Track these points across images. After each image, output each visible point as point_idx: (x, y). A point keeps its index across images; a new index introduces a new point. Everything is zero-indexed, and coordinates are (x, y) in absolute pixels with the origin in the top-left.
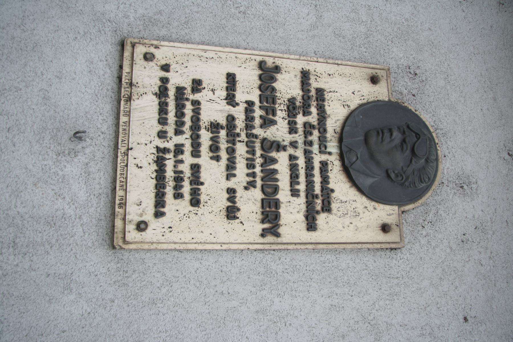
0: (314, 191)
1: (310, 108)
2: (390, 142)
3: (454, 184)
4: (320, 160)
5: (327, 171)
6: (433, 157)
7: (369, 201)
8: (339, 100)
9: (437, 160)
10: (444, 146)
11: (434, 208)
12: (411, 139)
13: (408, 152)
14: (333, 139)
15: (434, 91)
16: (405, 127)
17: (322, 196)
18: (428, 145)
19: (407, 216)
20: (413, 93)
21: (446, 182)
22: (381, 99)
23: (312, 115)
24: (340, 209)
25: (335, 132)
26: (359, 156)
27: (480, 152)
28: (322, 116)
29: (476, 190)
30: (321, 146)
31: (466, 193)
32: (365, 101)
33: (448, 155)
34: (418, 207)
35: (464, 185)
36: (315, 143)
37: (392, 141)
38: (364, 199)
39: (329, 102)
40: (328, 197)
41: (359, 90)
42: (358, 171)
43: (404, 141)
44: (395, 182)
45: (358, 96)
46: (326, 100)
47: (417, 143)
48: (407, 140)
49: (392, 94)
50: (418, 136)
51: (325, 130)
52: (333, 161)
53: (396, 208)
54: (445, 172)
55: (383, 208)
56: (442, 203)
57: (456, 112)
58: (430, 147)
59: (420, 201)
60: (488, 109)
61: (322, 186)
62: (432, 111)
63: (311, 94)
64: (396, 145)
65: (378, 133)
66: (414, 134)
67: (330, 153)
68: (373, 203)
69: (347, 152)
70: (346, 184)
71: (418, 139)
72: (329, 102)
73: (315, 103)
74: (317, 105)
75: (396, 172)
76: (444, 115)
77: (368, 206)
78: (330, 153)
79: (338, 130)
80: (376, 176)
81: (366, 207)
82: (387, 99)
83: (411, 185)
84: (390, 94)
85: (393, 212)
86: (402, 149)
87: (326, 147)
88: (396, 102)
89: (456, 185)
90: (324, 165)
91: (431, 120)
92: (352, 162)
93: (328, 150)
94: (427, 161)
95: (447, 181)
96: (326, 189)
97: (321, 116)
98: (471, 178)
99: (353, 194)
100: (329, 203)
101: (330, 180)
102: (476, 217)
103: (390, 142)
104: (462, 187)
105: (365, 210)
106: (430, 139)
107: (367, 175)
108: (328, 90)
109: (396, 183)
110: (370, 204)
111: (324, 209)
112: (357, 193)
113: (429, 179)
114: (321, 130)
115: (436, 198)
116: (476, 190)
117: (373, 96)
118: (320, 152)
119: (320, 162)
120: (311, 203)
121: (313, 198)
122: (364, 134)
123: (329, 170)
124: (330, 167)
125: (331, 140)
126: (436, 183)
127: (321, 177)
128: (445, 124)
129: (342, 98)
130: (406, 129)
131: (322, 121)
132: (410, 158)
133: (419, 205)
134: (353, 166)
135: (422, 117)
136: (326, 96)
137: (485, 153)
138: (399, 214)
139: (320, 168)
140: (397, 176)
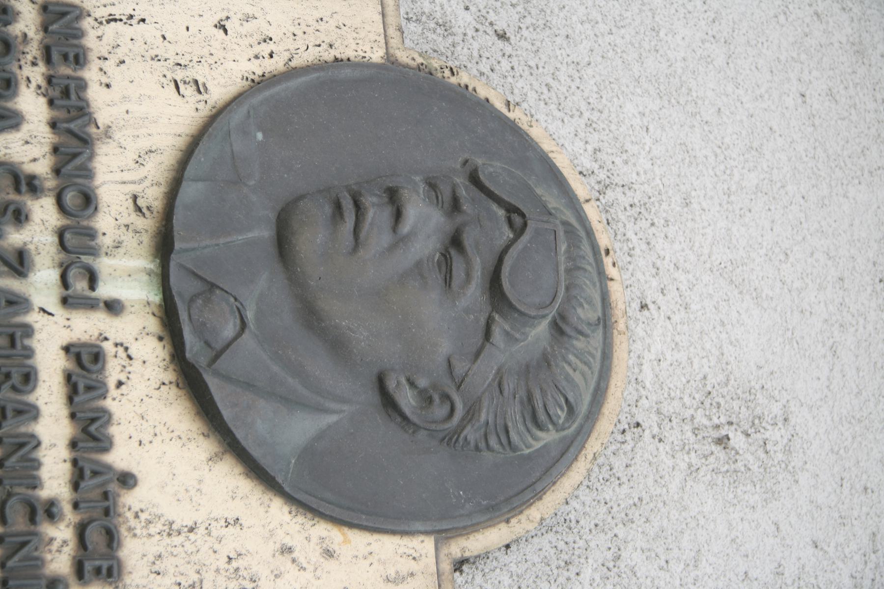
0: (35, 483)
1: (15, 94)
2: (393, 247)
3: (687, 428)
4: (67, 337)
5: (98, 389)
6: (586, 313)
7: (300, 519)
8: (155, 58)
9: (605, 322)
10: (641, 262)
11: (601, 540)
12: (488, 231)
13: (473, 294)
14: (129, 239)
15: (595, 15)
16: (461, 181)
17: (76, 506)
18: (562, 258)
19: (479, 579)
20: (500, 26)
21: (650, 422)
22: (350, 53)
23: (25, 127)
24: (167, 564)
25: (138, 209)
26: (250, 315)
27: (797, 284)
28: (75, 134)
29: (788, 451)
30: (72, 273)
31: (740, 465)
32: (277, 65)
33: (660, 299)
34: (528, 538)
35: (724, 435)
36: (38, 260)
37: (399, 242)
38: (278, 511)
39: (106, 65)
40: (107, 512)
41: (249, 10)
42: (249, 386)
43: (456, 241)
44: (417, 427)
45: (246, 42)
46: (92, 56)
47: (513, 252)
48: (468, 241)
49: (400, 29)
50: (517, 220)
51: (88, 200)
52: (128, 340)
53: (425, 545)
54: (648, 377)
55: (365, 550)
56: (634, 514)
57: (690, 108)
58: (574, 269)
59: (535, 512)
60: (830, 93)
61: (75, 462)
62: (583, 106)
63: (16, 29)
64: (418, 264)
65: (338, 207)
66: (501, 213)
67: (113, 307)
68: (322, 529)
69: (192, 300)
70: (192, 445)
71: (519, 232)
72: (106, 65)
73: (37, 74)
74: (49, 80)
75: (423, 383)
76: (637, 121)
77: (296, 541)
78: (113, 307)
79: (153, 196)
80: (333, 406)
81: (286, 550)
82: (377, 56)
83: (493, 442)
84: (391, 31)
85: (413, 566)
86: (448, 280)
87: (93, 279)
88: (419, 68)
89: (695, 431)
90: (85, 360)
91: (579, 144)
92: (218, 346)
93: (105, 290)
94: (559, 328)
95: (654, 417)
96: (95, 473)
97: (70, 132)
98: (761, 398)
99: (225, 487)
100: (111, 538)
101: (113, 430)
102: (790, 571)
103: (393, 247)
104: (722, 441)
105: (284, 563)
106: (570, 231)
107: (290, 402)
108: (102, 13)
109: (422, 435)
110: (308, 534)
111: (88, 566)
112: (245, 486)
113: (571, 410)
114: (70, 197)
115: (608, 494)
116: (788, 451)
117: (312, 40)
118: (65, 301)
119: (67, 349)
120: (24, 544)
121: (32, 518)
122: (272, 216)
123: (111, 383)
124: (113, 372)
125: (118, 245)
126: (604, 426)
127: (73, 416)
128: (644, 163)
129: (169, 51)
130: (465, 192)
131: (75, 156)
132: (483, 321)
133: (531, 527)
134: (222, 364)
135: (536, 132)
136: (90, 41)
137: (821, 288)
138: (439, 574)
139: (68, 377)
140: (426, 399)
